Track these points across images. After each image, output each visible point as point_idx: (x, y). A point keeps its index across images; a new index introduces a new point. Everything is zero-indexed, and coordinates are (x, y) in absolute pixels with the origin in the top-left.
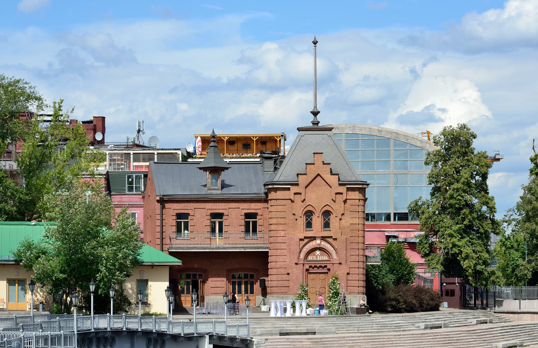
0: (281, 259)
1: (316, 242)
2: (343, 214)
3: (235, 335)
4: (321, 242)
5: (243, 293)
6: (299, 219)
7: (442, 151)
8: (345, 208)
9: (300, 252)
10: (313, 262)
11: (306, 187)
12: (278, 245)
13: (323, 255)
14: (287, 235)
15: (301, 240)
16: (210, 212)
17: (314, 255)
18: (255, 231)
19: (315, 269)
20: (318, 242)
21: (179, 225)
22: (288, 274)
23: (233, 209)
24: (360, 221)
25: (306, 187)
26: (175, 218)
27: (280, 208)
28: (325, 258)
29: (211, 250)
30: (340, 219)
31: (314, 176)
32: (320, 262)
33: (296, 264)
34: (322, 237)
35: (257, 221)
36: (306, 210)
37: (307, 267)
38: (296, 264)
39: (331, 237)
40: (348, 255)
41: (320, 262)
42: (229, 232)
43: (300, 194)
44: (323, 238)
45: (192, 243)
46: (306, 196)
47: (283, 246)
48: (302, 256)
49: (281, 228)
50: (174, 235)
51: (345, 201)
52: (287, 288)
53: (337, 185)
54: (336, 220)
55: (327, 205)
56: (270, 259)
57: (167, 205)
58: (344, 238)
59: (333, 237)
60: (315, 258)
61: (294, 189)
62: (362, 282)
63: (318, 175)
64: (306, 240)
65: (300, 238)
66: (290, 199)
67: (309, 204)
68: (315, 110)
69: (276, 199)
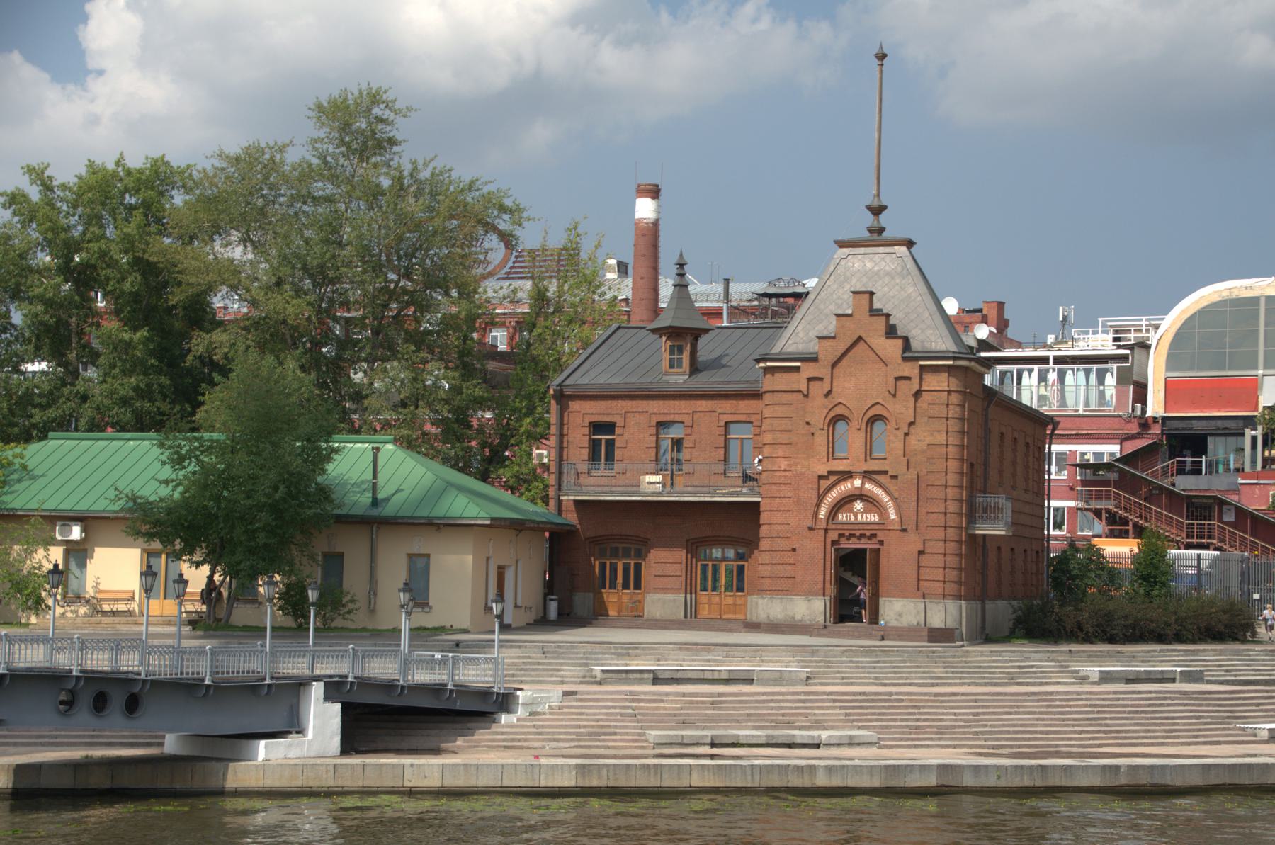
0: (779, 518)
1: (852, 484)
2: (911, 424)
3: (344, 671)
4: (863, 484)
5: (620, 586)
6: (818, 433)
7: (421, 278)
8: (918, 410)
9: (818, 505)
10: (856, 527)
11: (834, 365)
12: (775, 488)
13: (870, 512)
14: (793, 468)
15: (820, 477)
16: (588, 419)
17: (851, 511)
18: (610, 457)
19: (863, 540)
20: (858, 483)
21: (594, 447)
22: (794, 550)
23: (702, 414)
24: (950, 439)
25: (834, 365)
26: (586, 431)
27: (780, 411)
28: (874, 518)
29: (644, 499)
30: (906, 434)
31: (850, 342)
32: (861, 527)
33: (810, 529)
34: (865, 472)
35: (614, 440)
36: (832, 414)
37: (833, 536)
38: (810, 529)
39: (886, 473)
40: (922, 511)
41: (861, 527)
42: (694, 461)
43: (821, 379)
44: (867, 475)
45: (621, 483)
46: (834, 384)
47: (786, 491)
48: (822, 514)
49: (780, 453)
50: (583, 467)
51: (917, 394)
52: (791, 581)
53: (900, 360)
54: (896, 436)
55: (877, 403)
56: (764, 517)
57: (574, 405)
58: (912, 474)
59: (890, 473)
60: (853, 518)
61: (809, 370)
62: (955, 573)
63: (860, 338)
64: (833, 478)
65: (820, 474)
66: (800, 391)
67: (840, 400)
68: (876, 203)
69: (773, 392)
